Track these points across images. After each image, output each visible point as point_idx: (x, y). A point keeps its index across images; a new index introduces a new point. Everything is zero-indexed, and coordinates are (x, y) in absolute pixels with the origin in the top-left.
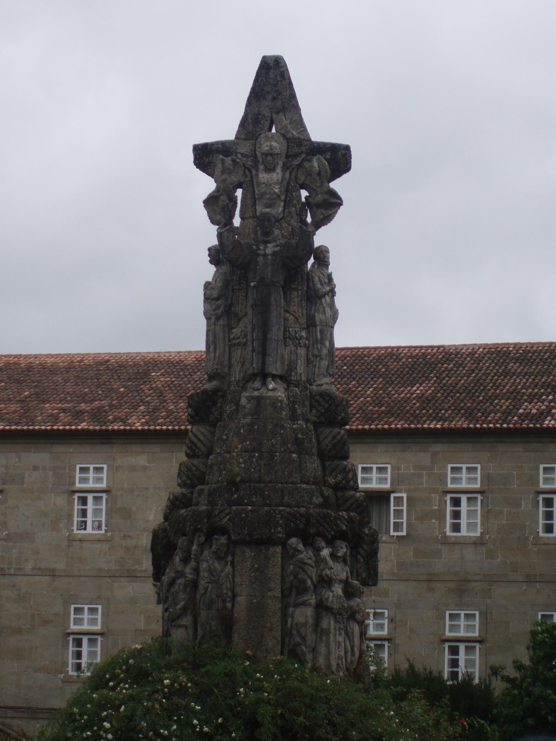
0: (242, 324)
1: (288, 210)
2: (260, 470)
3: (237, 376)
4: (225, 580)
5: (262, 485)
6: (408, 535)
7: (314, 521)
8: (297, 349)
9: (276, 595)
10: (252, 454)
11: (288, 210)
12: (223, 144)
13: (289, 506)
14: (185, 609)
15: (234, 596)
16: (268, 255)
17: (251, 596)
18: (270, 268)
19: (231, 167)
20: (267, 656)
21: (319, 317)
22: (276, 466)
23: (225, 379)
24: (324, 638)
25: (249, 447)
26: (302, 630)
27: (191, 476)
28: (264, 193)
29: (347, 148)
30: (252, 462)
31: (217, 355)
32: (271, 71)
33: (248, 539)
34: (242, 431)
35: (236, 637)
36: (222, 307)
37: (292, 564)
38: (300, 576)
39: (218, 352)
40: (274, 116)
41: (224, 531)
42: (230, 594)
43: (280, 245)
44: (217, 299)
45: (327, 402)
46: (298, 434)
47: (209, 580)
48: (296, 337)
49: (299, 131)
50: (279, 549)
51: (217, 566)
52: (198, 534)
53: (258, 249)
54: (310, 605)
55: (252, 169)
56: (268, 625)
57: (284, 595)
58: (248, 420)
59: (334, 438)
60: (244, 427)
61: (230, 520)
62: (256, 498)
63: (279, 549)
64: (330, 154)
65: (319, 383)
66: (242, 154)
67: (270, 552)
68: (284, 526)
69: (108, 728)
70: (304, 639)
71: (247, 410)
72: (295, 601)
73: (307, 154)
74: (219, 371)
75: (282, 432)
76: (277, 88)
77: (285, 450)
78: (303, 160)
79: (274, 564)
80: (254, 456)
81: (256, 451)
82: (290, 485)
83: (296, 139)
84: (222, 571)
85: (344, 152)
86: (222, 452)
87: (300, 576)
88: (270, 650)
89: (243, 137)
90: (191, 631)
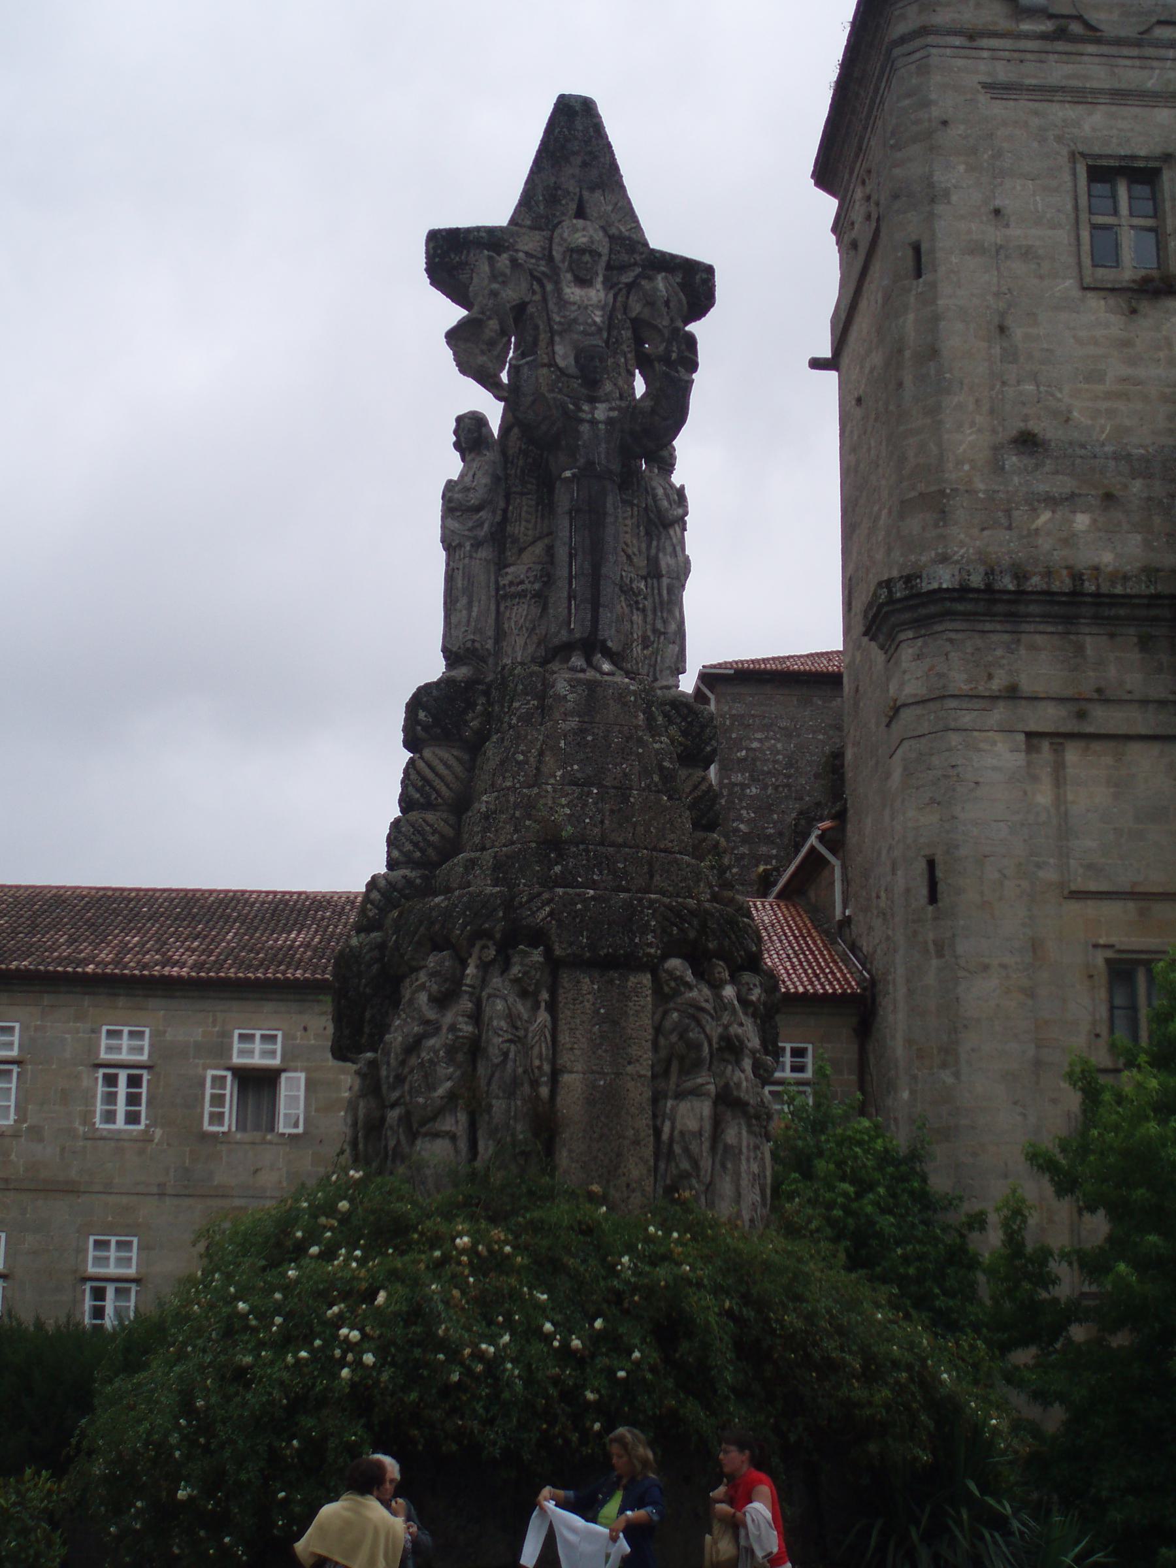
0: (526, 556)
1: (613, 360)
2: (602, 822)
3: (520, 654)
4: (537, 1038)
5: (611, 849)
6: (305, 1133)
7: (715, 926)
8: (632, 612)
9: (643, 1072)
10: (586, 789)
11: (613, 360)
12: (491, 231)
13: (663, 893)
14: (452, 1096)
15: (555, 1075)
16: (600, 422)
17: (593, 1072)
18: (604, 446)
19: (508, 271)
20: (628, 1198)
21: (666, 561)
22: (633, 816)
23: (485, 662)
24: (729, 1165)
25: (579, 775)
26: (694, 1147)
27: (422, 844)
28: (575, 321)
29: (710, 270)
30: (585, 805)
31: (474, 614)
32: (579, 118)
33: (588, 954)
34: (562, 744)
35: (563, 1158)
36: (486, 526)
37: (675, 1009)
38: (691, 1034)
39: (475, 609)
40: (586, 194)
41: (537, 937)
42: (547, 1068)
43: (619, 409)
44: (478, 509)
45: (684, 719)
46: (663, 760)
47: (510, 1037)
48: (632, 588)
49: (629, 227)
50: (646, 979)
51: (521, 1008)
52: (478, 945)
53: (580, 409)
54: (707, 1094)
55: (545, 281)
56: (630, 1133)
57: (661, 1072)
58: (573, 723)
59: (696, 787)
60: (565, 736)
61: (551, 914)
62: (601, 873)
63: (646, 979)
64: (681, 276)
65: (665, 683)
66: (526, 253)
67: (630, 984)
68: (659, 931)
69: (354, 1340)
70: (695, 1164)
71: (570, 705)
72: (678, 1086)
73: (644, 267)
74: (477, 645)
75: (640, 750)
76: (589, 148)
77: (648, 786)
78: (638, 277)
79: (639, 1008)
80: (590, 793)
81: (593, 785)
82: (663, 854)
83: (625, 239)
84: (529, 1022)
85: (705, 276)
86: (518, 785)
87: (691, 1034)
88: (634, 1185)
89: (528, 223)
90: (463, 1145)
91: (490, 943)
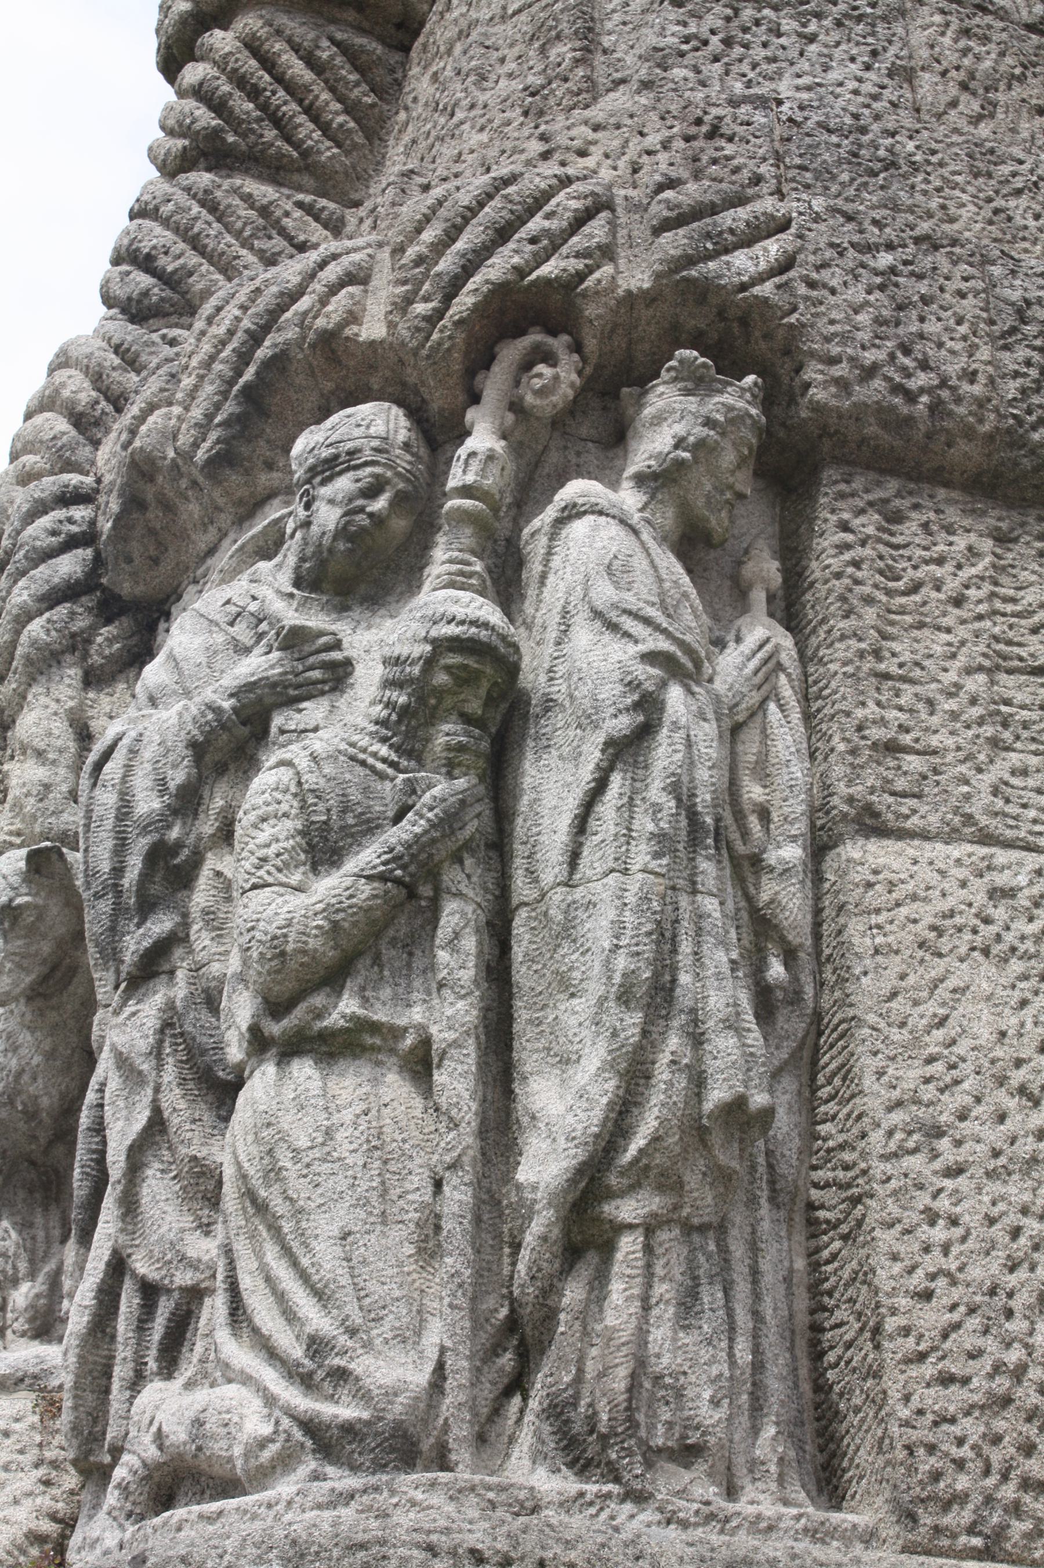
52: (511, 353)
91: (559, 344)
